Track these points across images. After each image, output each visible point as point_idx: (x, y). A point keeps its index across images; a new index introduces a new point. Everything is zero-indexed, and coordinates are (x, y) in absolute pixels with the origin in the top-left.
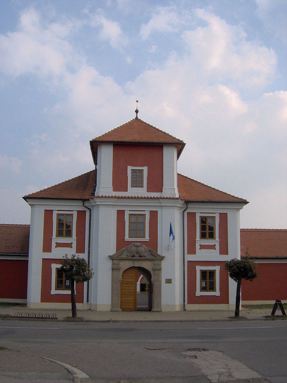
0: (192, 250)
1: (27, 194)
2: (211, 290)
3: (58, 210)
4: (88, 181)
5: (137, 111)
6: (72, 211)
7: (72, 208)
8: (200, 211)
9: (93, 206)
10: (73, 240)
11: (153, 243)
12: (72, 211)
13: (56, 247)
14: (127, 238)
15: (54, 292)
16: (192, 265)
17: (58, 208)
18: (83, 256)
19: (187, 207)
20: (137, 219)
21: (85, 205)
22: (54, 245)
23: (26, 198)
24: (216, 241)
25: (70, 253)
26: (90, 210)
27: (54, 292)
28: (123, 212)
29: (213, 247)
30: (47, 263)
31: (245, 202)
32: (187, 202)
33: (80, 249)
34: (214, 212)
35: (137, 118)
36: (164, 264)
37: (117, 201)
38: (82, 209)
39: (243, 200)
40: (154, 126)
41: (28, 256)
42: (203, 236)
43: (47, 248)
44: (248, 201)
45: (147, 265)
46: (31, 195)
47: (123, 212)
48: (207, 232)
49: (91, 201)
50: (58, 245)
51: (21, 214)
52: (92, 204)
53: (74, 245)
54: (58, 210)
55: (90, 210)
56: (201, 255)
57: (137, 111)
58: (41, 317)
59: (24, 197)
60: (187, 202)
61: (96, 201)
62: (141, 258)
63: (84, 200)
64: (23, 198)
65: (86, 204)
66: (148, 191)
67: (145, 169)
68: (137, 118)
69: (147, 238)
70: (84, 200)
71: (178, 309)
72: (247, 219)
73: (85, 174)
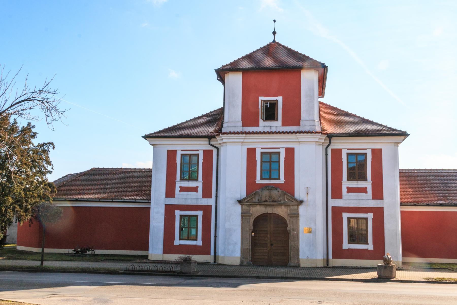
0: (337, 194)
1: (148, 133)
2: (261, 271)
3: (262, 148)
4: (217, 117)
5: (274, 33)
6: (366, 149)
7: (199, 146)
8: (346, 146)
9: (220, 144)
10: (199, 184)
11: (289, 187)
12: (366, 149)
13: (180, 191)
14: (258, 180)
15: (177, 242)
16: (337, 212)
17: (182, 146)
18: (211, 202)
19: (330, 143)
20: (270, 158)
21: (212, 143)
22: (177, 189)
23: (146, 137)
24: (368, 185)
25: (196, 198)
26: (218, 149)
27: (177, 242)
28: (174, 152)
29: (364, 190)
30: (170, 210)
31: (404, 134)
32: (330, 136)
33: (207, 194)
34: (365, 146)
35: (274, 41)
36: (302, 209)
37: (246, 138)
38: (210, 148)
39: (403, 132)
40: (293, 49)
41: (150, 202)
42: (351, 178)
43: (170, 193)
44: (408, 133)
45: (281, 211)
46: (152, 134)
47: (174, 152)
48: (357, 172)
49: (218, 139)
50: (183, 189)
51: (141, 157)
52: (219, 142)
53: (200, 189)
54: (262, 148)
55: (218, 149)
56: (348, 200)
57: (274, 33)
58: (164, 270)
59: (144, 136)
60: (330, 136)
61: (222, 138)
62: (276, 203)
63: (210, 138)
64: (143, 137)
65: (213, 142)
66: (283, 125)
67: (280, 99)
68: (274, 41)
69: (282, 180)
70: (210, 138)
71: (321, 264)
72: (412, 156)
73: (218, 109)
